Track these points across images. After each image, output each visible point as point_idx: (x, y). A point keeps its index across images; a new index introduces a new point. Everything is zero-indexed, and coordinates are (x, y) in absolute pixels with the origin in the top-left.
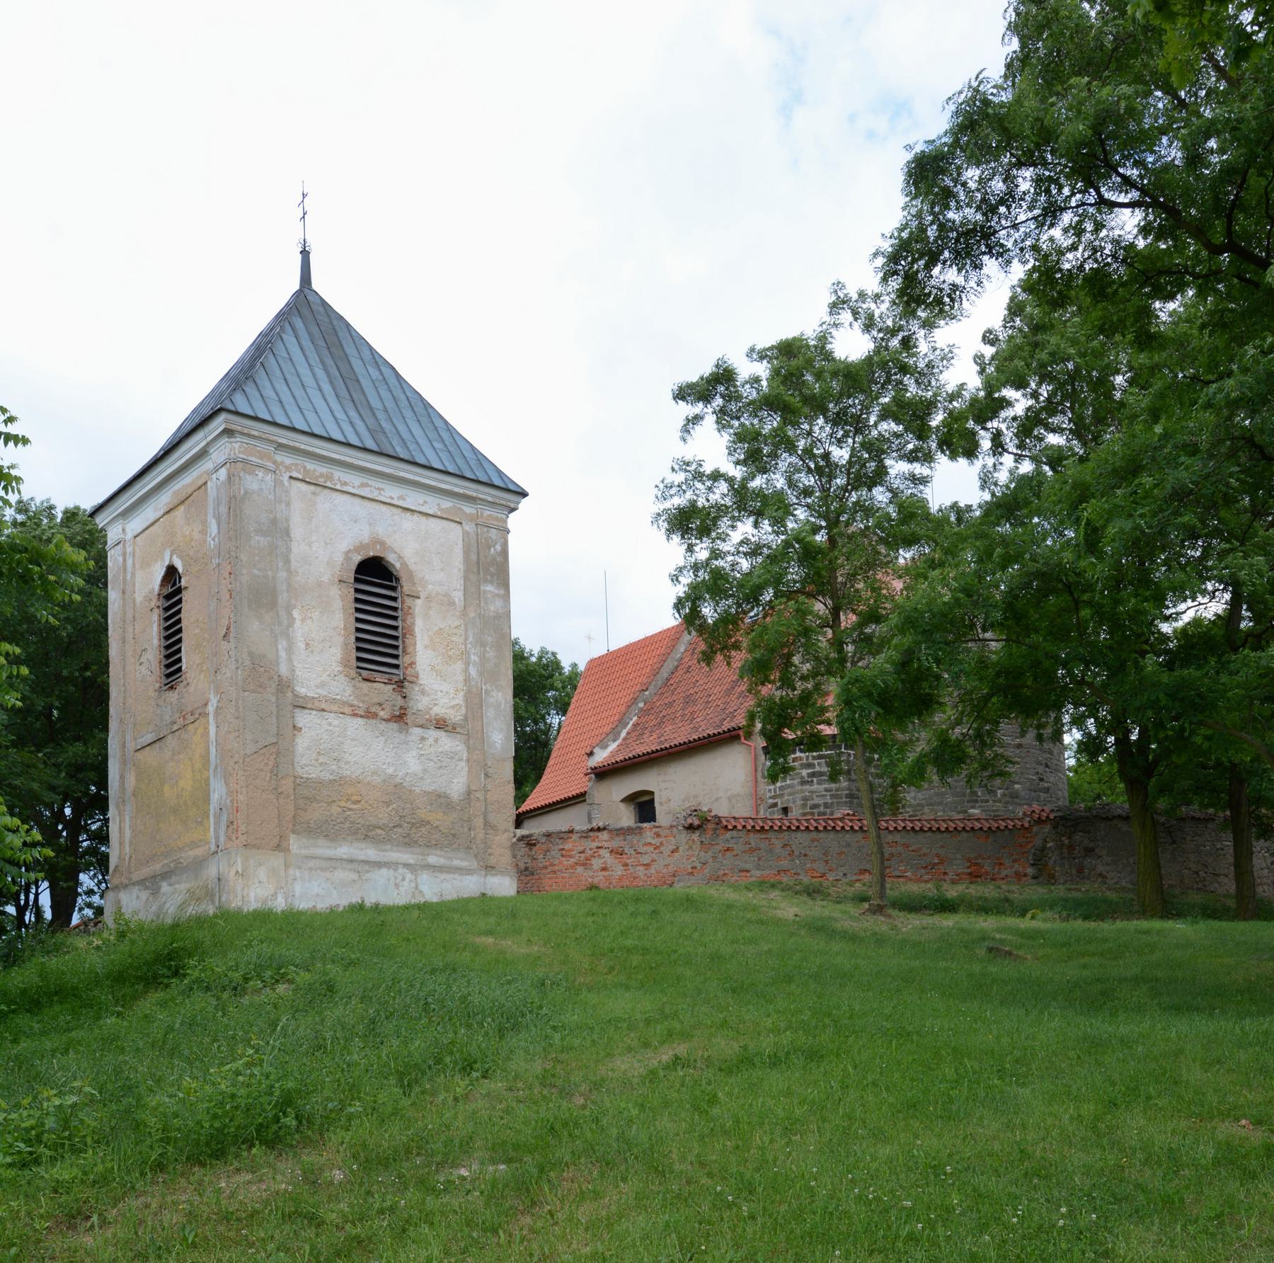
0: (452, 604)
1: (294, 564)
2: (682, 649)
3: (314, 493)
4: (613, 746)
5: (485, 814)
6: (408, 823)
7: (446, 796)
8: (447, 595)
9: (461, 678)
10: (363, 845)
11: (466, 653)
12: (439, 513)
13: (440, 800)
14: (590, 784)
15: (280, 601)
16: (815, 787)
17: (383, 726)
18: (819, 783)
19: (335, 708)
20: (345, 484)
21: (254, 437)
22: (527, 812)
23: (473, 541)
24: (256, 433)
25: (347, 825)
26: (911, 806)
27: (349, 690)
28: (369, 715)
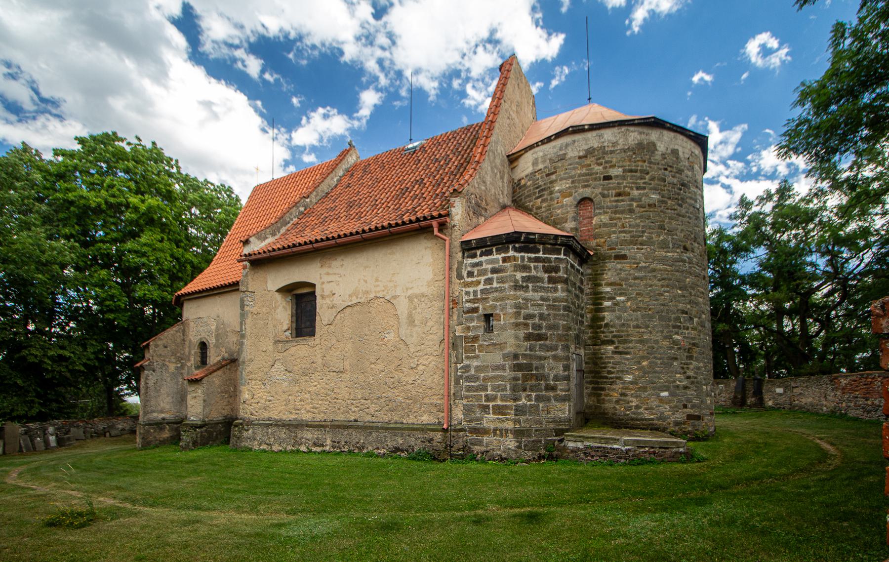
2: (341, 173)
4: (270, 240)
14: (244, 272)
16: (530, 294)
18: (534, 290)
22: (189, 294)
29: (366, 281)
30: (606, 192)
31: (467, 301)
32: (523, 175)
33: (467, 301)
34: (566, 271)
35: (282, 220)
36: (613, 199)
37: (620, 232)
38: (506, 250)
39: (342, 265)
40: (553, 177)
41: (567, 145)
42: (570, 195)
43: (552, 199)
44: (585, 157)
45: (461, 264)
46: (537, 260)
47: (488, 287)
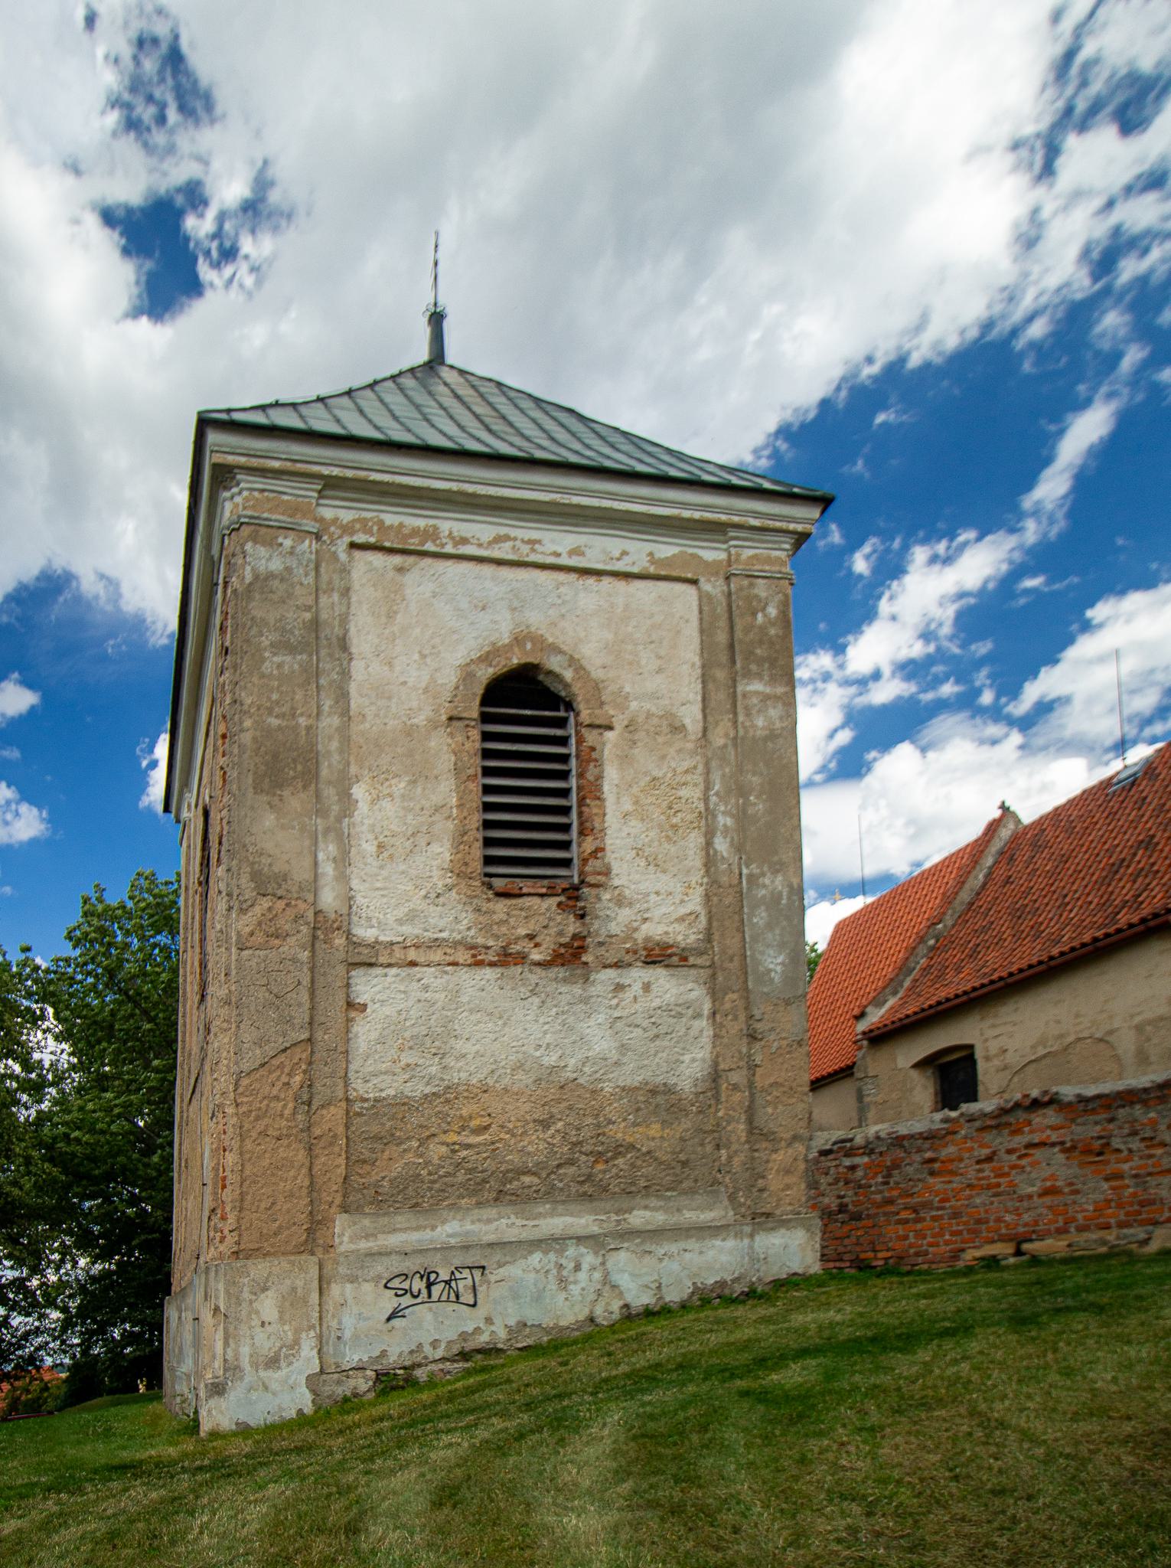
0: (678, 729)
1: (355, 703)
3: (400, 570)
5: (750, 1112)
6: (591, 1159)
7: (669, 1090)
8: (669, 716)
9: (698, 863)
10: (491, 1212)
11: (709, 814)
12: (652, 570)
13: (657, 1099)
15: (324, 772)
17: (536, 976)
19: (437, 956)
20: (464, 541)
21: (278, 474)
23: (721, 609)
24: (276, 464)
25: (461, 1177)
27: (467, 918)
28: (507, 958)
29: (1058, 1022)
35: (903, 969)
39: (1016, 1010)
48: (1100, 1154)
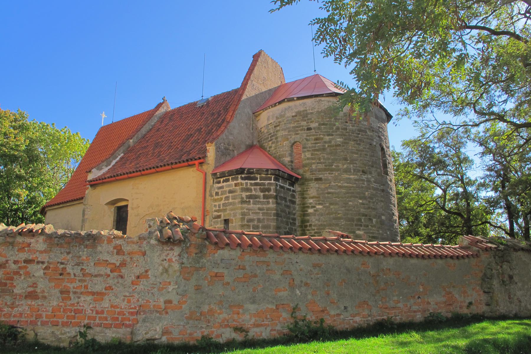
18: (254, 204)
26: (314, 226)
30: (308, 138)
31: (216, 211)
32: (262, 126)
33: (216, 211)
34: (276, 191)
36: (312, 142)
37: (318, 163)
38: (237, 179)
40: (278, 128)
41: (286, 109)
42: (288, 139)
43: (277, 142)
44: (296, 116)
45: (212, 187)
46: (256, 184)
47: (227, 202)
48: (61, 274)
